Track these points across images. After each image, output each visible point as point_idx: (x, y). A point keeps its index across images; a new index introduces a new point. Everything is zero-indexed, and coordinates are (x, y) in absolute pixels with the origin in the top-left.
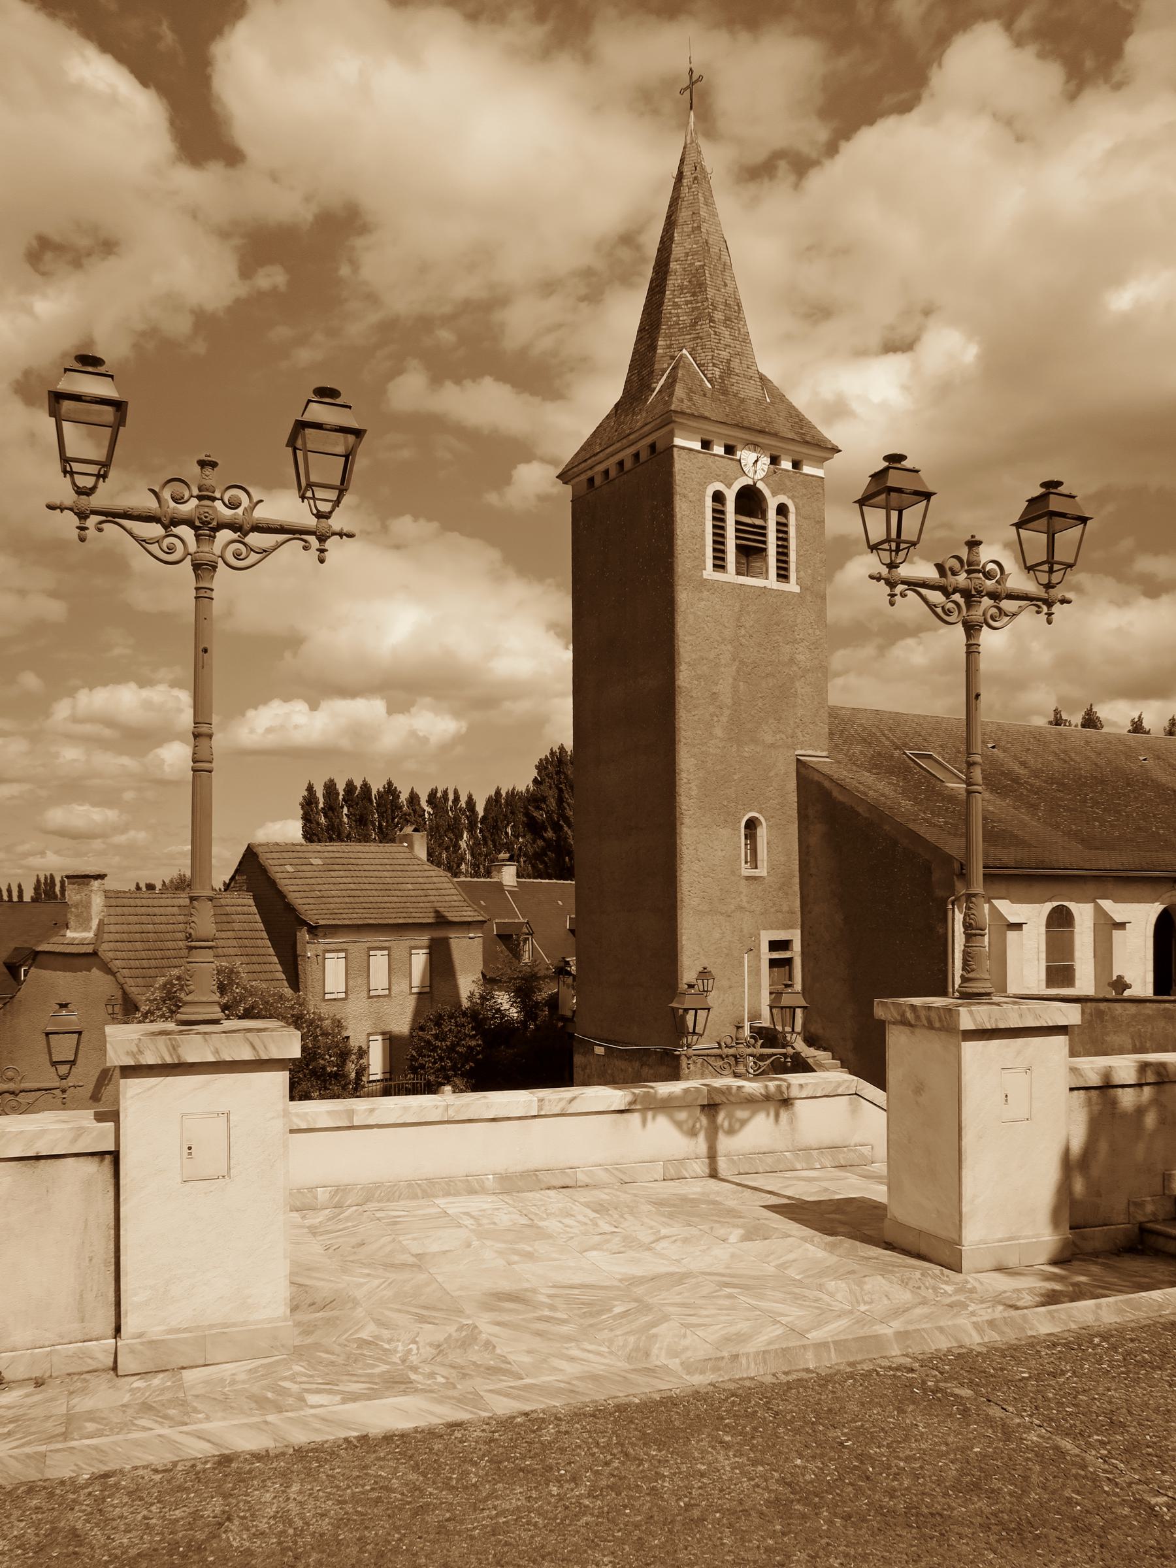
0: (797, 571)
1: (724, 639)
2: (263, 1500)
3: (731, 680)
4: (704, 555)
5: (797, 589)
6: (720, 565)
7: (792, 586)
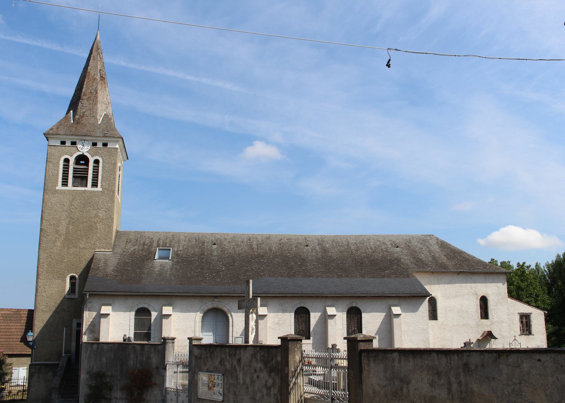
4: (58, 181)
5: (101, 190)
6: (65, 183)
7: (99, 189)
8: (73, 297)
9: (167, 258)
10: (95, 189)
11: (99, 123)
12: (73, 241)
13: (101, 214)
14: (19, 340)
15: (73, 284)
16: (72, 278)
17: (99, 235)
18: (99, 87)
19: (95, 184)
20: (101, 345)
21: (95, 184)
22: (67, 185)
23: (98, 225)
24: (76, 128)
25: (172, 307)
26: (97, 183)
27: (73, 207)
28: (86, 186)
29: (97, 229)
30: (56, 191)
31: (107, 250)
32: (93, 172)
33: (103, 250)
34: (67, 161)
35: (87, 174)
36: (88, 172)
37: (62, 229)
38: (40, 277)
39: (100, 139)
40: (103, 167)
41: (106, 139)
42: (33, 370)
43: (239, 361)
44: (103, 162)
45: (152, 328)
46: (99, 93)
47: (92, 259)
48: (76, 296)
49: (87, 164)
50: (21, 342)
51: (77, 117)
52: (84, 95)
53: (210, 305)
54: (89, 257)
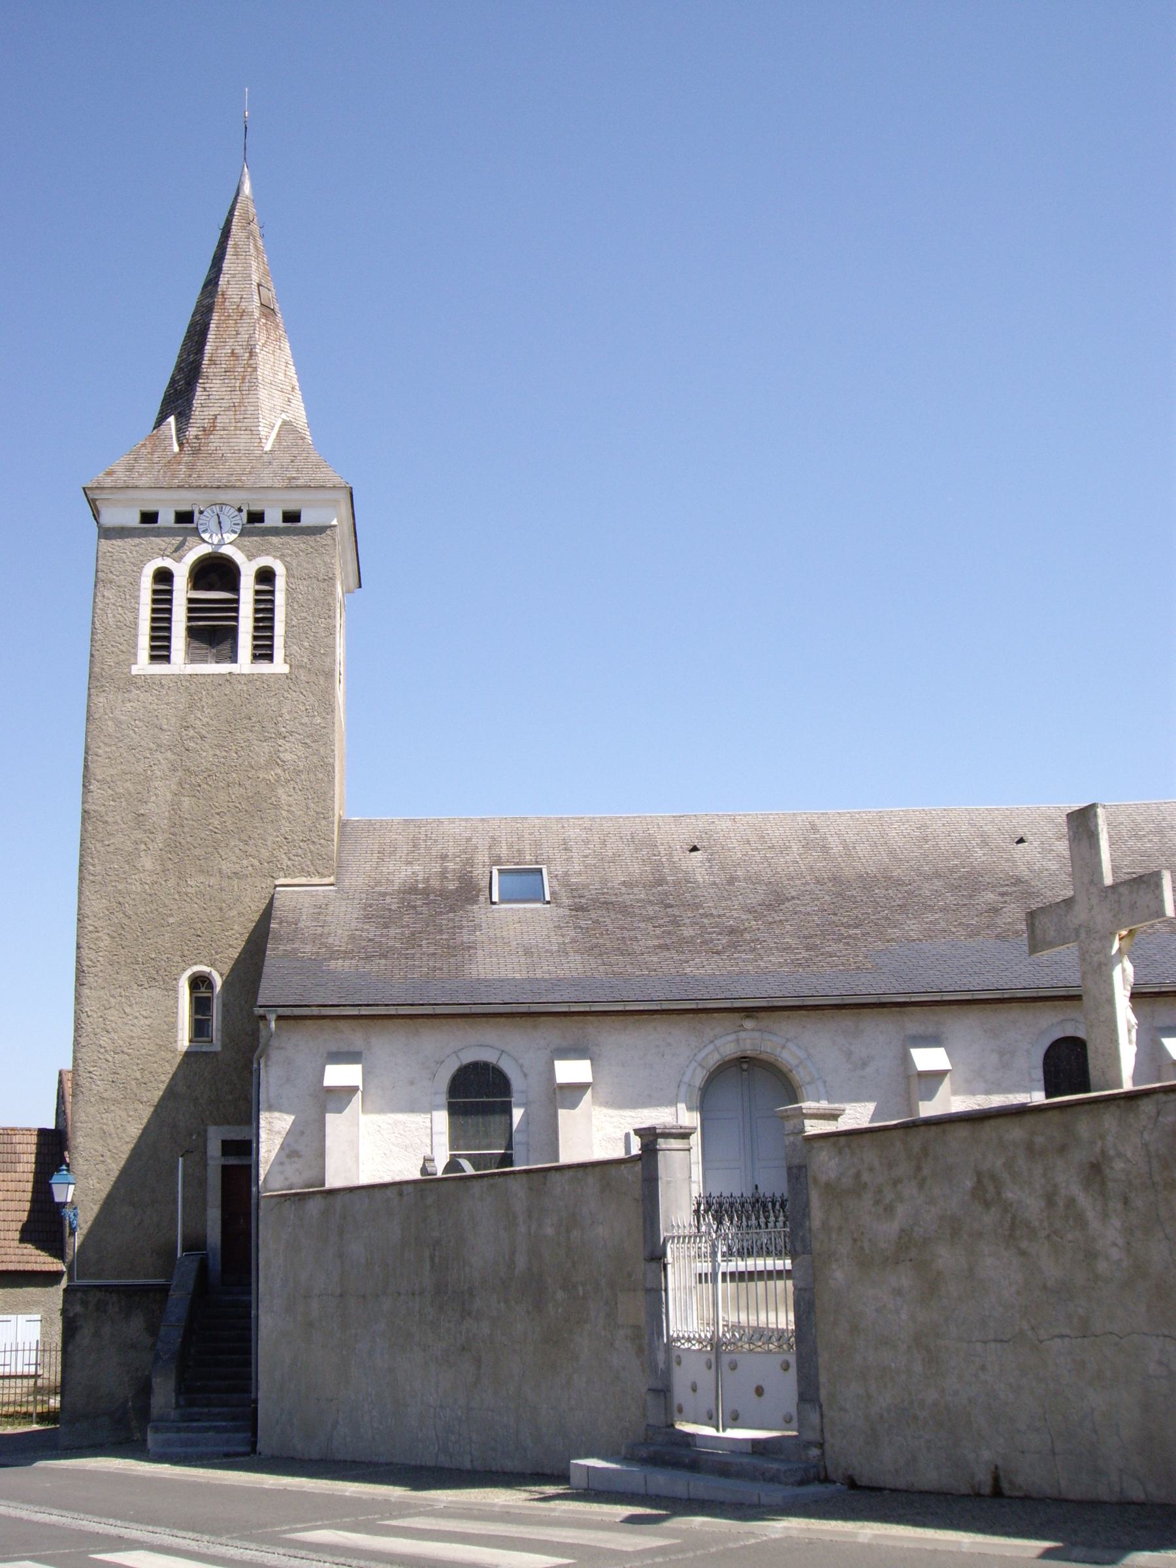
0: (286, 646)
1: (159, 746)
2: (118, 1095)
3: (169, 797)
4: (135, 646)
5: (285, 669)
6: (161, 652)
7: (279, 666)
8: (205, 1048)
9: (539, 897)
10: (264, 668)
11: (268, 448)
12: (197, 852)
13: (291, 752)
14: (17, 1235)
15: (200, 1006)
16: (199, 983)
17: (286, 827)
18: (260, 337)
19: (263, 652)
20: (339, 1200)
21: (263, 652)
22: (167, 659)
23: (280, 791)
24: (191, 467)
25: (588, 1062)
26: (271, 647)
27: (191, 733)
28: (234, 659)
29: (277, 807)
30: (133, 682)
31: (316, 880)
32: (257, 611)
33: (303, 880)
34: (164, 577)
35: (236, 619)
36: (236, 610)
37: (158, 807)
38: (90, 979)
39: (273, 495)
40: (289, 592)
41: (296, 495)
42: (78, 1308)
43: (1095, 1172)
44: (289, 575)
45: (516, 1138)
46: (262, 356)
47: (267, 914)
48: (217, 1046)
49: (232, 583)
50: (22, 1240)
51: (192, 432)
52: (213, 362)
53: (727, 1042)
54: (253, 909)
